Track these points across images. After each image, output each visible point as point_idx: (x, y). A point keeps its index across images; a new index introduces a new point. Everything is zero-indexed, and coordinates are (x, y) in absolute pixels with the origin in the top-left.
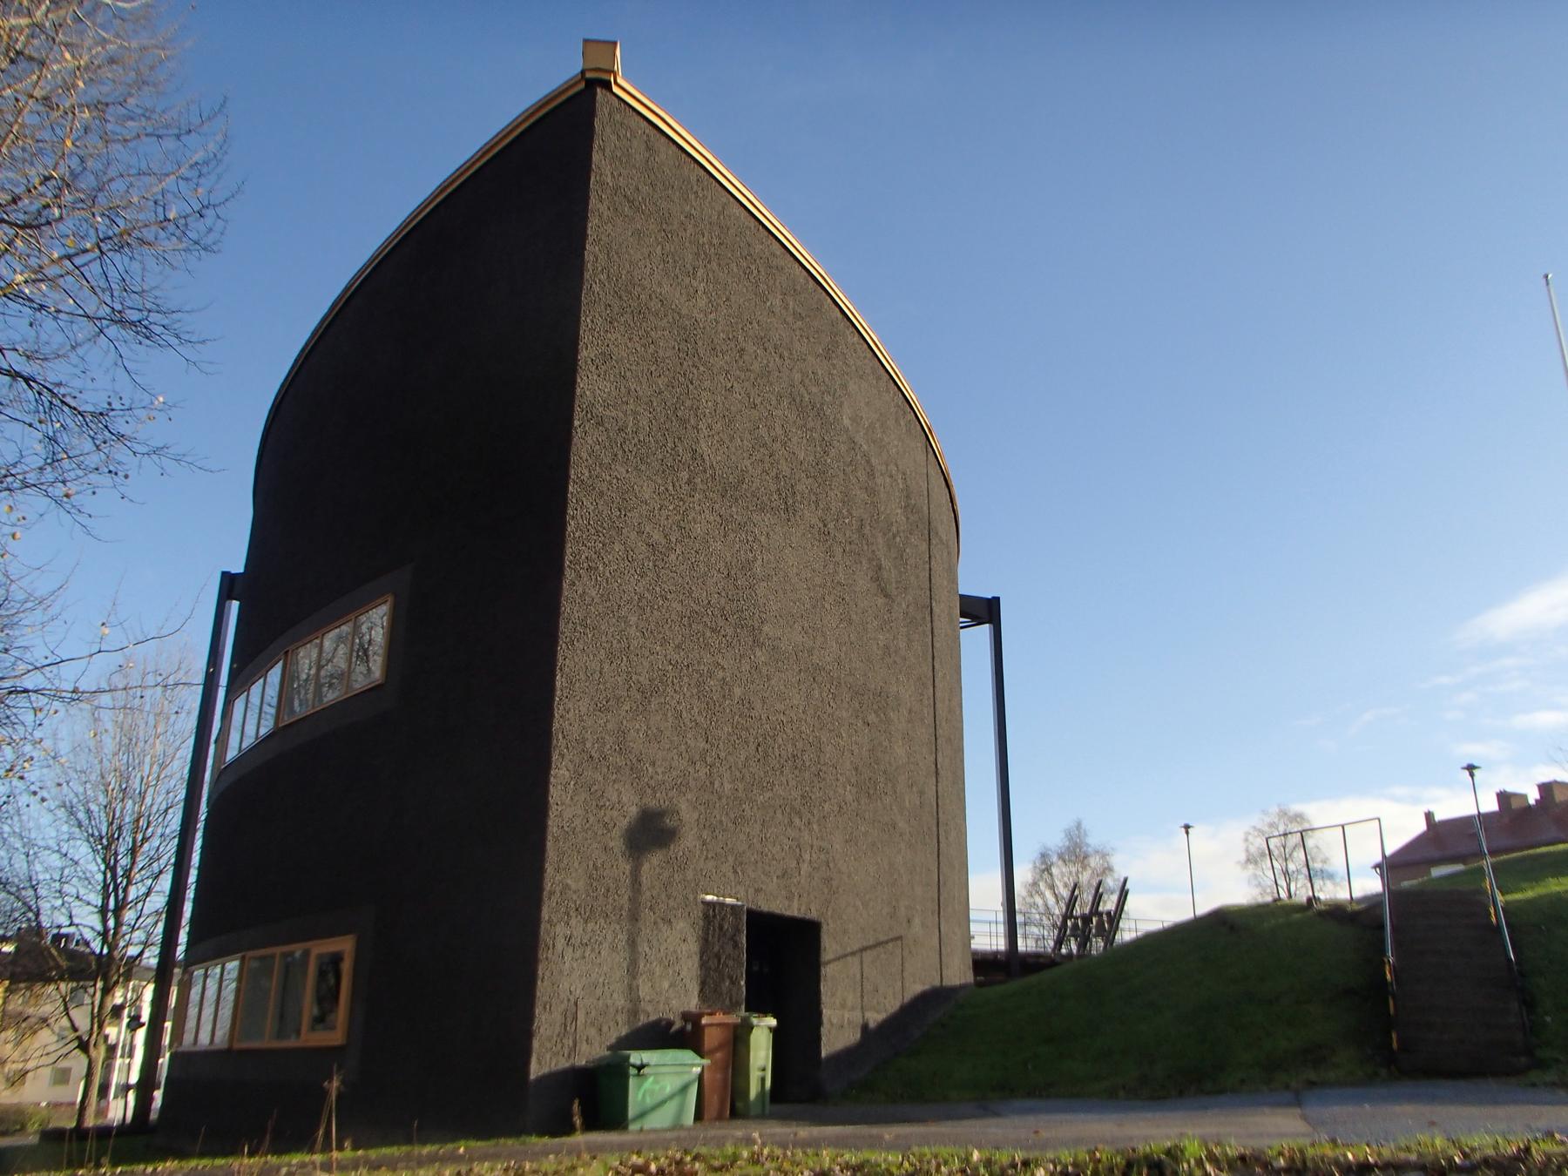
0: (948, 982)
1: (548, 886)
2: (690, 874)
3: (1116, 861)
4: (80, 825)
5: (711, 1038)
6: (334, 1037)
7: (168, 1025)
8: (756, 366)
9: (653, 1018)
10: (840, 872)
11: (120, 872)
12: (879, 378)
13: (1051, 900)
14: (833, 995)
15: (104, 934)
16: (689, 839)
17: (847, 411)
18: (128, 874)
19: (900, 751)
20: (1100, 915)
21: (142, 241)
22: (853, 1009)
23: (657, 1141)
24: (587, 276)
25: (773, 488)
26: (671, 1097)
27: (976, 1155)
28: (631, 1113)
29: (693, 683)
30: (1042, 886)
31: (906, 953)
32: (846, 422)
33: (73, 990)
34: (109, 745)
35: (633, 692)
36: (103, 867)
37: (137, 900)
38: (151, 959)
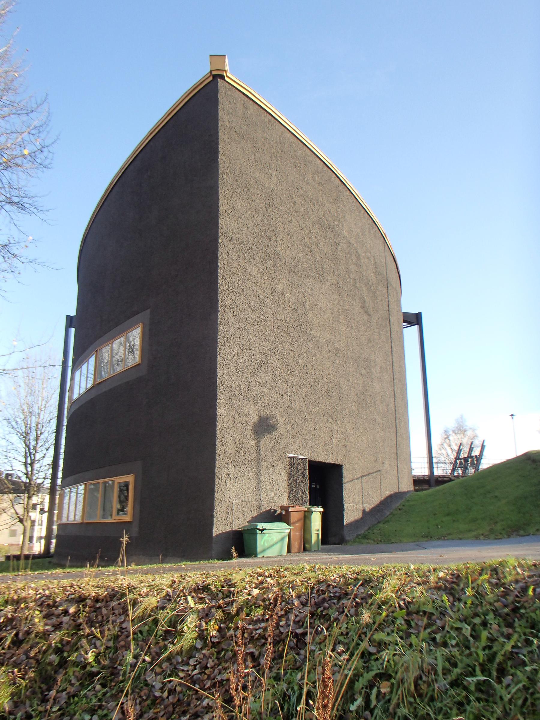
0: (401, 490)
1: (218, 451)
2: (282, 445)
3: (478, 433)
4: (13, 428)
5: (294, 517)
6: (127, 518)
7: (56, 512)
8: (302, 210)
9: (267, 509)
10: (351, 442)
11: (32, 447)
12: (360, 212)
13: (449, 452)
14: (349, 497)
15: (27, 474)
16: (281, 430)
17: (346, 228)
18: (35, 449)
19: (377, 386)
20: (472, 457)
21: (18, 165)
22: (358, 503)
23: (271, 561)
24: (220, 171)
25: (313, 266)
26: (276, 543)
27: (412, 567)
28: (259, 549)
29: (280, 359)
30: (445, 445)
31: (382, 478)
32: (346, 234)
33: (16, 497)
34: (23, 393)
35: (253, 364)
36: (24, 446)
37: (40, 459)
38: (47, 484)
